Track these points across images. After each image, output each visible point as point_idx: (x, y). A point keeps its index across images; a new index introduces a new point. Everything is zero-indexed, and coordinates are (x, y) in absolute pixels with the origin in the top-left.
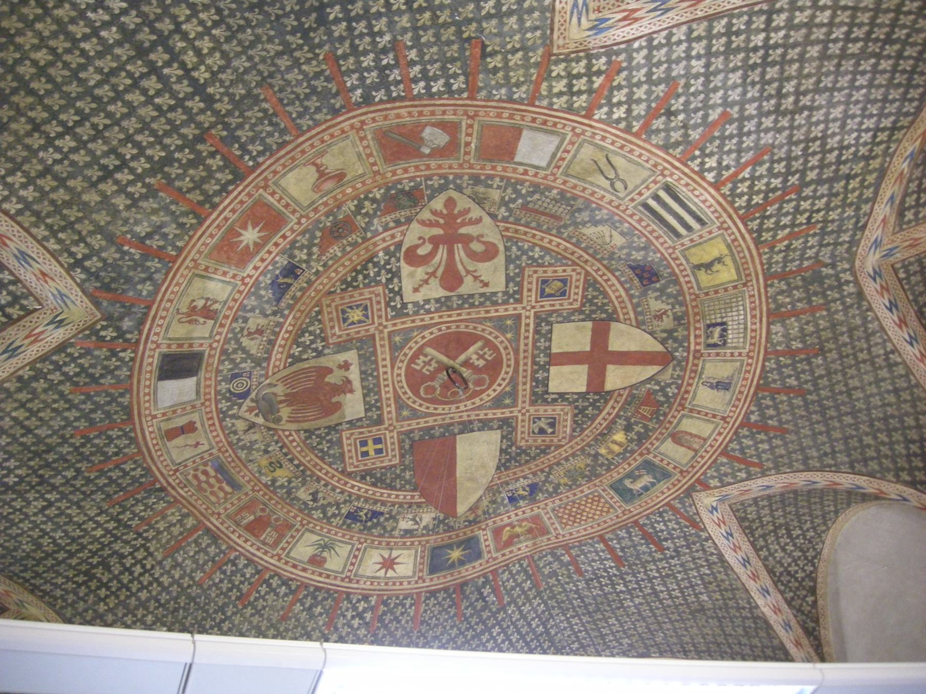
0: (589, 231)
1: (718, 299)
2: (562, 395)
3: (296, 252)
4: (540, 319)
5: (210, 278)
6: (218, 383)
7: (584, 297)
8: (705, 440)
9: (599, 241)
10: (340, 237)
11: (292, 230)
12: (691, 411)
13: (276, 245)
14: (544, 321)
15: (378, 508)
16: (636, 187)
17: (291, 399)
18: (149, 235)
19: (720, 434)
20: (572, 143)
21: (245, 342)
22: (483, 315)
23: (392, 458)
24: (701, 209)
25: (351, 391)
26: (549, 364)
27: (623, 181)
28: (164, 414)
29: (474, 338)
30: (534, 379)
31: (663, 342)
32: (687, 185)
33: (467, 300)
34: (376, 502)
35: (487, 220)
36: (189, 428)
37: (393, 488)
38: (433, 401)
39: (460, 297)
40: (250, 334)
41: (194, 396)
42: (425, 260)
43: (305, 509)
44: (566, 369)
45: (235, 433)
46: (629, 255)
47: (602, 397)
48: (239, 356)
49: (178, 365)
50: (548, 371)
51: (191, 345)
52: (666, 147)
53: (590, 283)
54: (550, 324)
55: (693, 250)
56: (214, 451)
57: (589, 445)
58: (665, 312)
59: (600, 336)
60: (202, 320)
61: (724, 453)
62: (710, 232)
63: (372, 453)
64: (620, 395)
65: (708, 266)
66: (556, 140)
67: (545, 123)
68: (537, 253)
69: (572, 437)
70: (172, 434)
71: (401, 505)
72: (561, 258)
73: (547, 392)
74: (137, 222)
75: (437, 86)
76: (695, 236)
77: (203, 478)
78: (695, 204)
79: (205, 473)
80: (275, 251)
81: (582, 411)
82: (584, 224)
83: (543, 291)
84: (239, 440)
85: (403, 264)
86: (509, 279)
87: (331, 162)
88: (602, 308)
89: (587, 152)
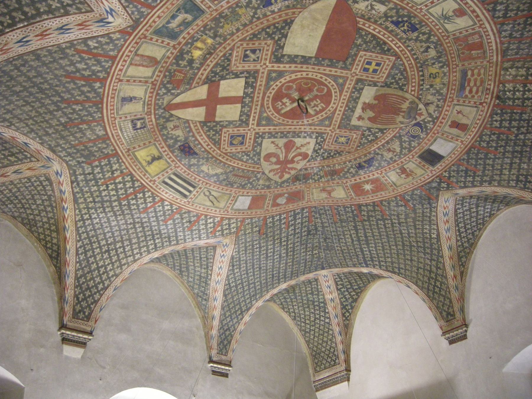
0: (219, 171)
1: (142, 140)
2: (237, 76)
3: (354, 172)
4: (246, 123)
5: (393, 182)
6: (423, 139)
7: (221, 135)
8: (131, 64)
9: (214, 167)
10: (333, 171)
11: (351, 181)
12: (146, 82)
13: (360, 179)
14: (244, 122)
15: (392, 27)
16: (199, 194)
17: (397, 111)
18: (402, 206)
19: (121, 70)
20: (228, 207)
21: (398, 150)
22: (277, 128)
23: (363, 56)
24: (167, 189)
25: (364, 103)
26: (243, 98)
27: (206, 195)
28: (457, 140)
29: (287, 115)
30: (254, 88)
31: (172, 115)
32: (177, 199)
33: (284, 135)
34: (391, 32)
35: (267, 172)
36: (455, 125)
37: (374, 36)
38: (321, 83)
39: (287, 137)
40: (394, 152)
41: (438, 139)
42: (300, 154)
43: (438, 44)
44: (233, 94)
45: (437, 106)
46: (198, 161)
47: (210, 80)
48: (405, 145)
49: (431, 158)
50: (244, 93)
51: (420, 163)
52: (189, 212)
53: (217, 143)
54: (240, 120)
55: (165, 167)
56: (455, 102)
57: (220, 44)
58: (172, 130)
59: (211, 114)
60: (408, 170)
61: (113, 58)
62: (159, 178)
63: (374, 64)
64: (198, 83)
65: (154, 159)
66: (235, 207)
67: (239, 213)
68: (245, 158)
69: (232, 49)
70: (463, 127)
71: (375, 22)
72: (233, 156)
73: (246, 77)
74: (402, 211)
75: (277, 218)
76: (166, 175)
77: (474, 89)
78: (171, 191)
79: (471, 91)
80: (362, 177)
81: (224, 68)
82: (222, 174)
83: (243, 138)
84: (439, 100)
85: (310, 154)
86: (260, 145)
87: (324, 195)
88: (210, 128)
89: (222, 205)
